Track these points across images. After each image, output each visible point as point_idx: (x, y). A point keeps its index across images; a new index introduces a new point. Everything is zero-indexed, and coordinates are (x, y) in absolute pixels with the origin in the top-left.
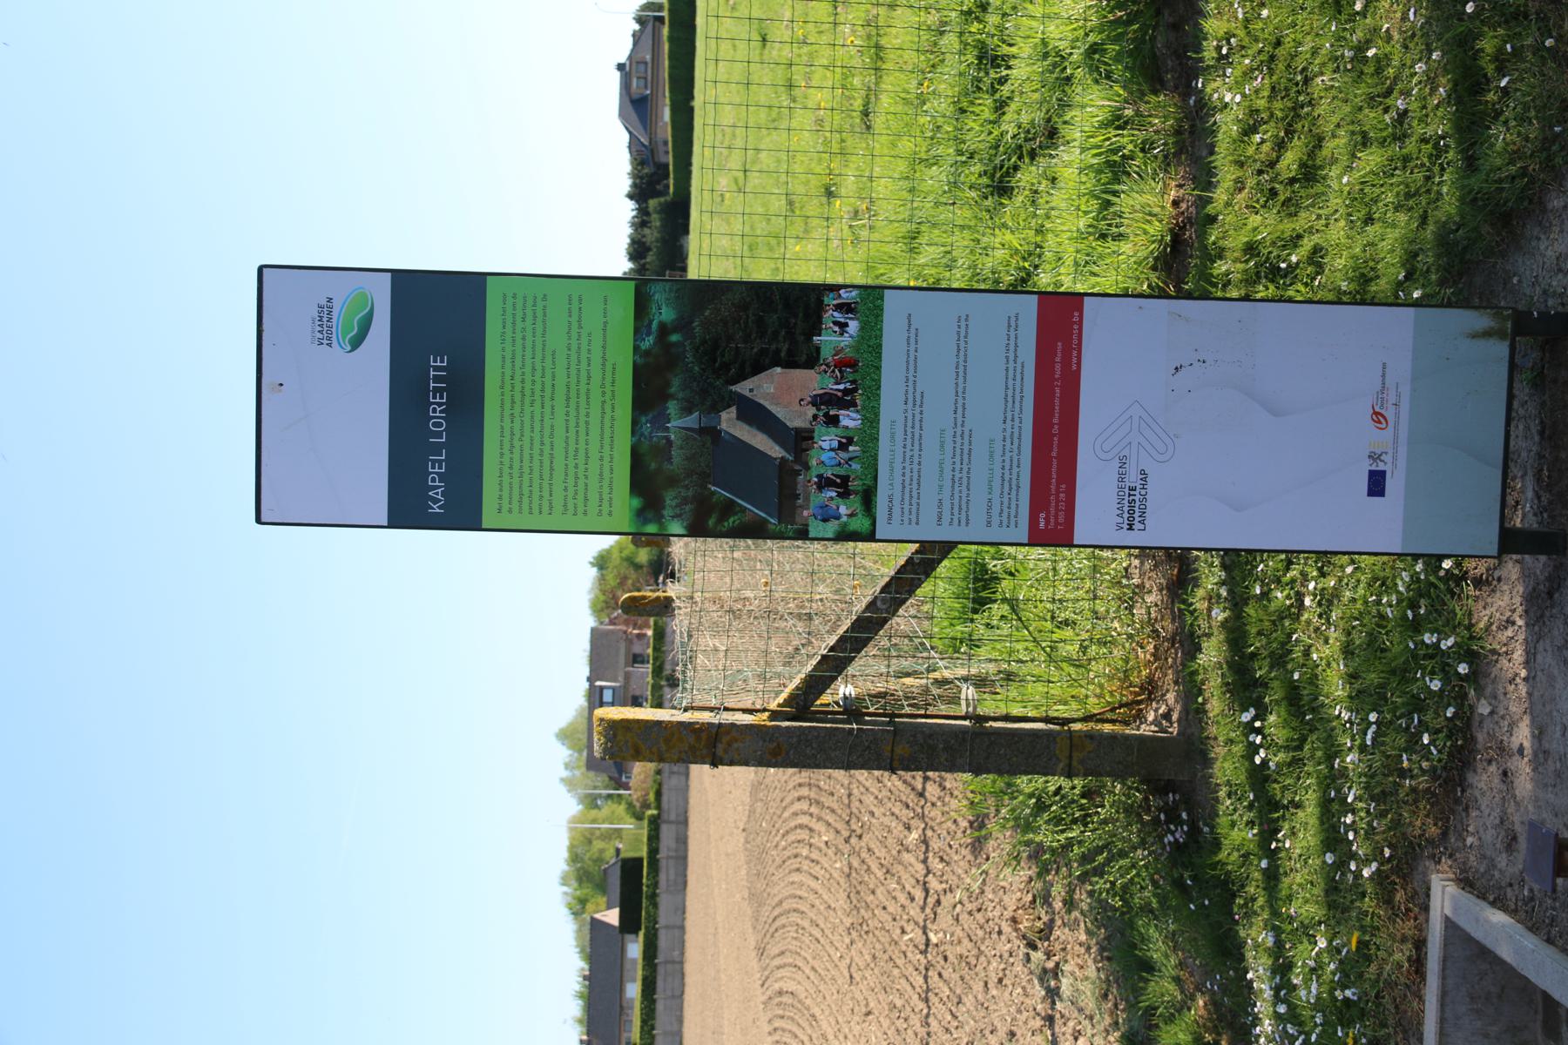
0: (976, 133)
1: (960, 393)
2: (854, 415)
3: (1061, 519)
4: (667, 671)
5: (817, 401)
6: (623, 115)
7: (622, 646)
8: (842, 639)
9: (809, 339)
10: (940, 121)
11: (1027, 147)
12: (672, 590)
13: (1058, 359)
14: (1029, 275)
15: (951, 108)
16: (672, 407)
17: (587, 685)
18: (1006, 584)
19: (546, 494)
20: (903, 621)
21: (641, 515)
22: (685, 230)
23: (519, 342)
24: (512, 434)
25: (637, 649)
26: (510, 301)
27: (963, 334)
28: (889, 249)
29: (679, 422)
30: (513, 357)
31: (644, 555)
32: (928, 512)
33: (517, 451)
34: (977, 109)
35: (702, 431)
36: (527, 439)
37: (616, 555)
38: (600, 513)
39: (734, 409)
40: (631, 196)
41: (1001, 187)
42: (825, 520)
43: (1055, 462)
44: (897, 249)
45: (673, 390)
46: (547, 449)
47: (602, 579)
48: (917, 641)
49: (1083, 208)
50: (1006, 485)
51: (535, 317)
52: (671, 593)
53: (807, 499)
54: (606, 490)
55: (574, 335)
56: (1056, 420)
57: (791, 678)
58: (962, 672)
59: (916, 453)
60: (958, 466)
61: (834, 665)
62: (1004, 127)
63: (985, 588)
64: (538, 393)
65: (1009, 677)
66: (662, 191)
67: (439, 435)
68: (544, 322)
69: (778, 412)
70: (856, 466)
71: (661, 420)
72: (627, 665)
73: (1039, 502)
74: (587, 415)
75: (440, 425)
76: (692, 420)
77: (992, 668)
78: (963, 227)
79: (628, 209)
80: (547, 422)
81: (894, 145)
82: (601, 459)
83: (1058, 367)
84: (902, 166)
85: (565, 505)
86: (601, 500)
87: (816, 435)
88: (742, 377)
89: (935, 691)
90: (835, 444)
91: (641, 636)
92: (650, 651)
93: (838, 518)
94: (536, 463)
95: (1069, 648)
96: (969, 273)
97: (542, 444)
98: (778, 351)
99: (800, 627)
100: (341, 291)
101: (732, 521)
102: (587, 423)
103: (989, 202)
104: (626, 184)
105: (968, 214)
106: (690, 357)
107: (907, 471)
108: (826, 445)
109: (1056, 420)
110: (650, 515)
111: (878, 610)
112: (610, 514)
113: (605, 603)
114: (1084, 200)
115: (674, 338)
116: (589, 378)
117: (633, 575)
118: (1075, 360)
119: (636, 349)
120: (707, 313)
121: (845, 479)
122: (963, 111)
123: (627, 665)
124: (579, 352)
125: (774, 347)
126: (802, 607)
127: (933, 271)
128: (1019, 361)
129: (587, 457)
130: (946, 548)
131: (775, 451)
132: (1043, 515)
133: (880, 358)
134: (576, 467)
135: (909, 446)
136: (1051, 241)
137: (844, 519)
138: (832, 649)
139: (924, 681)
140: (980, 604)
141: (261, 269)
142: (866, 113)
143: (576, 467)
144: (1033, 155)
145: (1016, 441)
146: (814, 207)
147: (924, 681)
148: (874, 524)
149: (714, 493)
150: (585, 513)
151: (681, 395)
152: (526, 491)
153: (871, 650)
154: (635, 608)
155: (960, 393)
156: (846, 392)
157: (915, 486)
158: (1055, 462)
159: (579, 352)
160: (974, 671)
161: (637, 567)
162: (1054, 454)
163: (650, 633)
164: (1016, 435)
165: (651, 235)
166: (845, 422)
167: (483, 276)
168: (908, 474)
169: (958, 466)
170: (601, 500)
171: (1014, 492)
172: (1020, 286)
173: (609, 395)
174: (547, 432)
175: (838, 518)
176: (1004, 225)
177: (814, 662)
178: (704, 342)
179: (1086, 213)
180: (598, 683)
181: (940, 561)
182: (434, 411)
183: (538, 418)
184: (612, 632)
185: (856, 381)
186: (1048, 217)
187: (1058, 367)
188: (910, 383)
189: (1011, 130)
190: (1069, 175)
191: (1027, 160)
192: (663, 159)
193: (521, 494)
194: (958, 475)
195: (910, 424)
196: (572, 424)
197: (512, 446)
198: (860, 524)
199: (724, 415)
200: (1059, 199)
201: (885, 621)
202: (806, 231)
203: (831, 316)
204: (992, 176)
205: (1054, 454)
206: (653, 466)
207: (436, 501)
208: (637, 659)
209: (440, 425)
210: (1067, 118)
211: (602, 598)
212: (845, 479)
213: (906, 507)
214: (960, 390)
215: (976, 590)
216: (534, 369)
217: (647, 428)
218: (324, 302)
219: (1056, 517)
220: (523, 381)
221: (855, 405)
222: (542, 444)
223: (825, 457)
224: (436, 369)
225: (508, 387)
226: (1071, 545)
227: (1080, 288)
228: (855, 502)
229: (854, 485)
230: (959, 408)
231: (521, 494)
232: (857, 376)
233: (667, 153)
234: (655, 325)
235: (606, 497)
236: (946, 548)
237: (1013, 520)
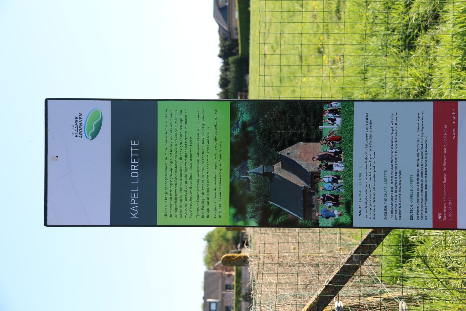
0: (396, 19)
1: (394, 152)
2: (340, 165)
3: (450, 216)
4: (244, 292)
5: (323, 158)
6: (215, 16)
7: (220, 281)
8: (335, 277)
9: (317, 127)
10: (377, 14)
11: (424, 24)
12: (246, 252)
13: (445, 134)
14: (425, 90)
15: (383, 7)
16: (250, 163)
17: (202, 301)
18: (419, 249)
19: (188, 207)
20: (367, 268)
21: (235, 217)
22: (247, 72)
23: (174, 133)
24: (171, 178)
25: (228, 282)
26: (169, 113)
27: (394, 122)
28: (353, 79)
29: (253, 170)
30: (171, 141)
31: (230, 235)
32: (380, 213)
33: (174, 186)
34: (395, 7)
35: (265, 174)
36: (178, 181)
37: (216, 234)
38: (215, 216)
39: (280, 163)
40: (220, 56)
41: (409, 44)
42: (327, 218)
43: (445, 186)
44: (356, 79)
45: (250, 154)
46: (188, 185)
47: (209, 247)
48: (373, 278)
49: (454, 55)
50: (420, 198)
51: (181, 120)
52: (247, 255)
53: (318, 207)
54: (218, 205)
55: (201, 129)
56: (445, 165)
57: (310, 298)
58: (398, 294)
59: (372, 183)
60: (394, 189)
61: (332, 291)
62: (411, 15)
63: (408, 250)
64: (184, 158)
65: (424, 297)
66: (235, 54)
67: (136, 179)
68: (186, 123)
69: (302, 164)
70: (342, 190)
71: (244, 169)
72: (223, 290)
73: (437, 207)
74: (208, 168)
75: (136, 175)
76: (259, 169)
77: (414, 292)
78: (389, 67)
79: (219, 62)
80: (188, 172)
81: (353, 27)
82: (215, 189)
83: (445, 138)
84: (357, 37)
85: (198, 213)
86: (215, 210)
87: (321, 175)
88: (284, 147)
89: (385, 304)
90: (331, 179)
91: (229, 276)
92: (234, 283)
93: (334, 216)
94: (183, 193)
95: (455, 281)
96: (394, 90)
97: (186, 183)
98: (301, 134)
99: (313, 270)
100: (86, 110)
101: (281, 219)
102: (208, 172)
103: (403, 54)
104: (217, 50)
105: (392, 60)
106: (258, 138)
107: (368, 192)
108: (326, 180)
109: (445, 165)
110: (240, 217)
111: (353, 262)
112: (220, 216)
113: (211, 259)
114: (455, 51)
115: (250, 129)
116: (208, 150)
117: (225, 244)
118: (454, 134)
119: (231, 135)
120: (266, 116)
121: (337, 197)
122: (389, 8)
123: (223, 290)
124: (203, 138)
125: (299, 132)
126: (314, 260)
127: (375, 90)
128: (424, 135)
129: (208, 189)
130: (387, 231)
131: (301, 183)
132: (440, 214)
133: (352, 135)
134: (203, 193)
135: (368, 180)
136: (437, 73)
137: (337, 217)
138: (330, 282)
139: (379, 299)
140: (406, 258)
141: (46, 101)
142: (338, 11)
143: (203, 193)
144: (426, 28)
145: (424, 176)
146: (312, 60)
147: (379, 299)
148: (352, 219)
149: (271, 205)
150: (208, 216)
151: (254, 157)
152: (178, 206)
153: (349, 283)
154: (228, 262)
155: (394, 152)
156: (336, 153)
157: (372, 200)
158: (445, 186)
159: (203, 138)
160: (404, 294)
161: (227, 241)
162: (445, 182)
163: (234, 273)
164: (424, 173)
165: (230, 75)
166: (335, 168)
167: (154, 102)
168: (369, 194)
169: (394, 189)
170: (215, 210)
171: (424, 202)
172: (420, 97)
173: (218, 157)
174: (188, 176)
175: (334, 216)
176: (412, 65)
177: (321, 289)
178: (265, 130)
179: (456, 57)
180: (209, 300)
181: (385, 237)
182: (133, 168)
183: (184, 170)
184: (214, 274)
185: (341, 146)
186: (435, 60)
187: (445, 138)
188: (368, 148)
189: (415, 16)
190: (446, 38)
191: (423, 31)
192: (235, 37)
193: (176, 208)
194: (394, 194)
195: (368, 169)
196: (201, 172)
197: (171, 184)
198: (345, 219)
199: (275, 166)
200: (441, 50)
201: (357, 268)
202: (309, 71)
203: (327, 116)
204: (405, 41)
205: (445, 182)
206: (241, 192)
207: (134, 212)
208: (228, 287)
209: (136, 175)
210: (445, 9)
211: (210, 256)
212: (337, 197)
213: (368, 210)
214: (394, 151)
215: (403, 252)
216: (181, 146)
217: (237, 174)
218: (78, 116)
219: (447, 214)
220: (176, 152)
221: (341, 160)
222: (186, 183)
223: (326, 186)
224: (134, 147)
225: (169, 155)
226: (455, 228)
227: (454, 96)
228: (342, 208)
229: (341, 200)
230: (394, 160)
231: (176, 208)
232: (341, 145)
233: (237, 34)
234: (240, 123)
235: (218, 208)
236: (387, 231)
237: (424, 216)
